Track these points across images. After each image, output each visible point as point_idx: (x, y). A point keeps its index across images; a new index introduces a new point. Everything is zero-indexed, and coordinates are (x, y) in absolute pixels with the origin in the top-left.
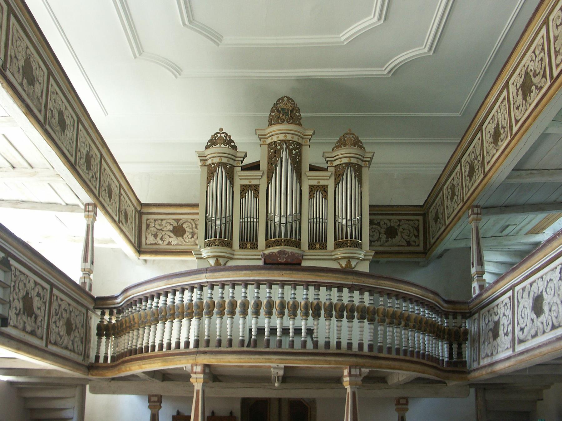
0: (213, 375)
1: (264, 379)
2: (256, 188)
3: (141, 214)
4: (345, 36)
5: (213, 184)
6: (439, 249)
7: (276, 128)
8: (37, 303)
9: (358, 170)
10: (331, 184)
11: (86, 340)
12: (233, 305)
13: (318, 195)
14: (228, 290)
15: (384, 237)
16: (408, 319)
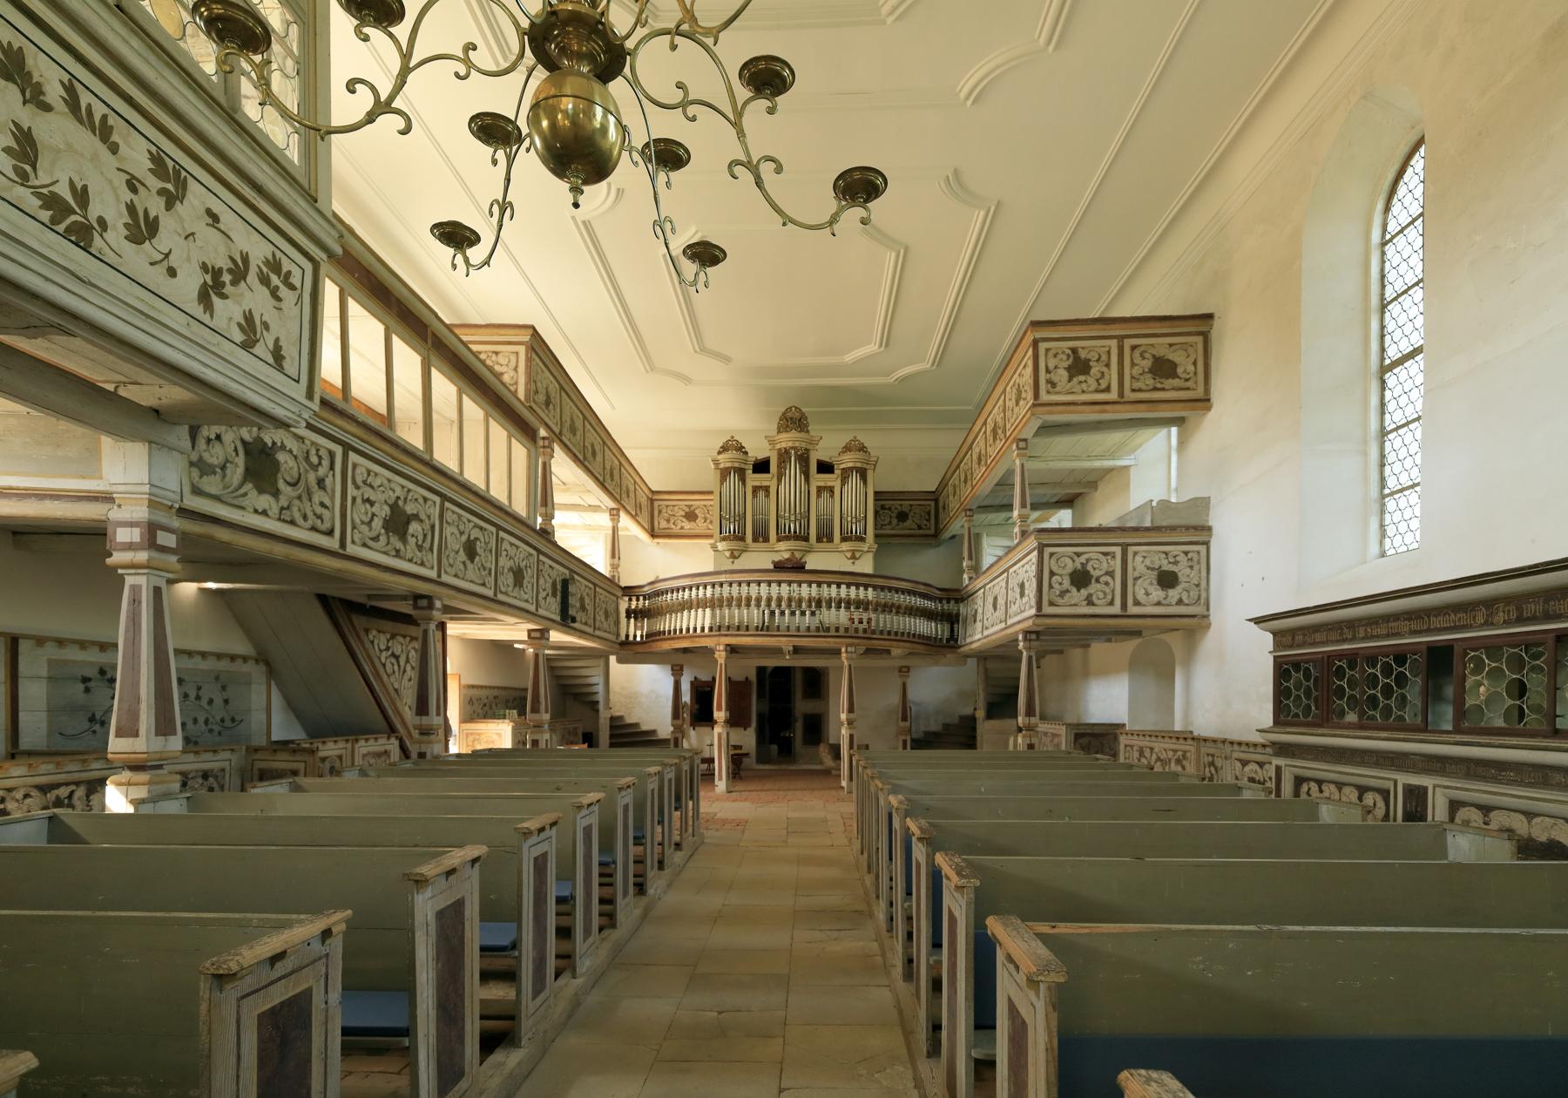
0: (732, 650)
1: (777, 651)
2: (767, 489)
3: (652, 501)
4: (849, 358)
5: (726, 484)
6: (947, 535)
7: (784, 436)
8: (587, 601)
9: (863, 474)
10: (837, 485)
11: (617, 623)
12: (749, 599)
13: (825, 495)
14: (744, 587)
15: (895, 521)
16: (899, 607)
